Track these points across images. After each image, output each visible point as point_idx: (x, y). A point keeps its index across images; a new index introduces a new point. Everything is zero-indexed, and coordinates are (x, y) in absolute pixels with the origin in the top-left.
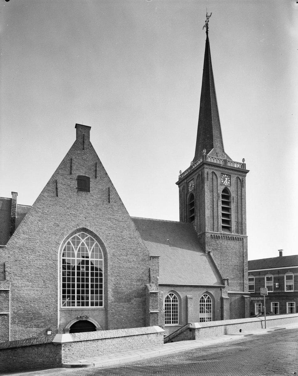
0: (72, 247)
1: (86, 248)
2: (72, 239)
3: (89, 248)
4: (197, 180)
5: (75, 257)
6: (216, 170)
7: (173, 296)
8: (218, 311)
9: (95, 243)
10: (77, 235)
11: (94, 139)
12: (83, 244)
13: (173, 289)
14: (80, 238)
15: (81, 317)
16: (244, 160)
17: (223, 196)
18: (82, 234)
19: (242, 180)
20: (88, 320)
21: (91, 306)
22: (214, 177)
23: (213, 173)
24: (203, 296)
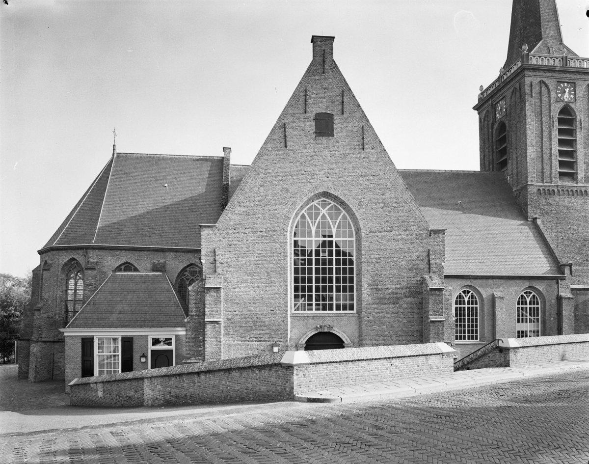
2: (308, 209)
6: (547, 77)
7: (531, 295)
8: (552, 319)
9: (342, 214)
10: (314, 203)
12: (324, 217)
13: (468, 282)
14: (320, 207)
15: (321, 327)
20: (332, 331)
21: (336, 310)
22: (544, 88)
24: (523, 293)
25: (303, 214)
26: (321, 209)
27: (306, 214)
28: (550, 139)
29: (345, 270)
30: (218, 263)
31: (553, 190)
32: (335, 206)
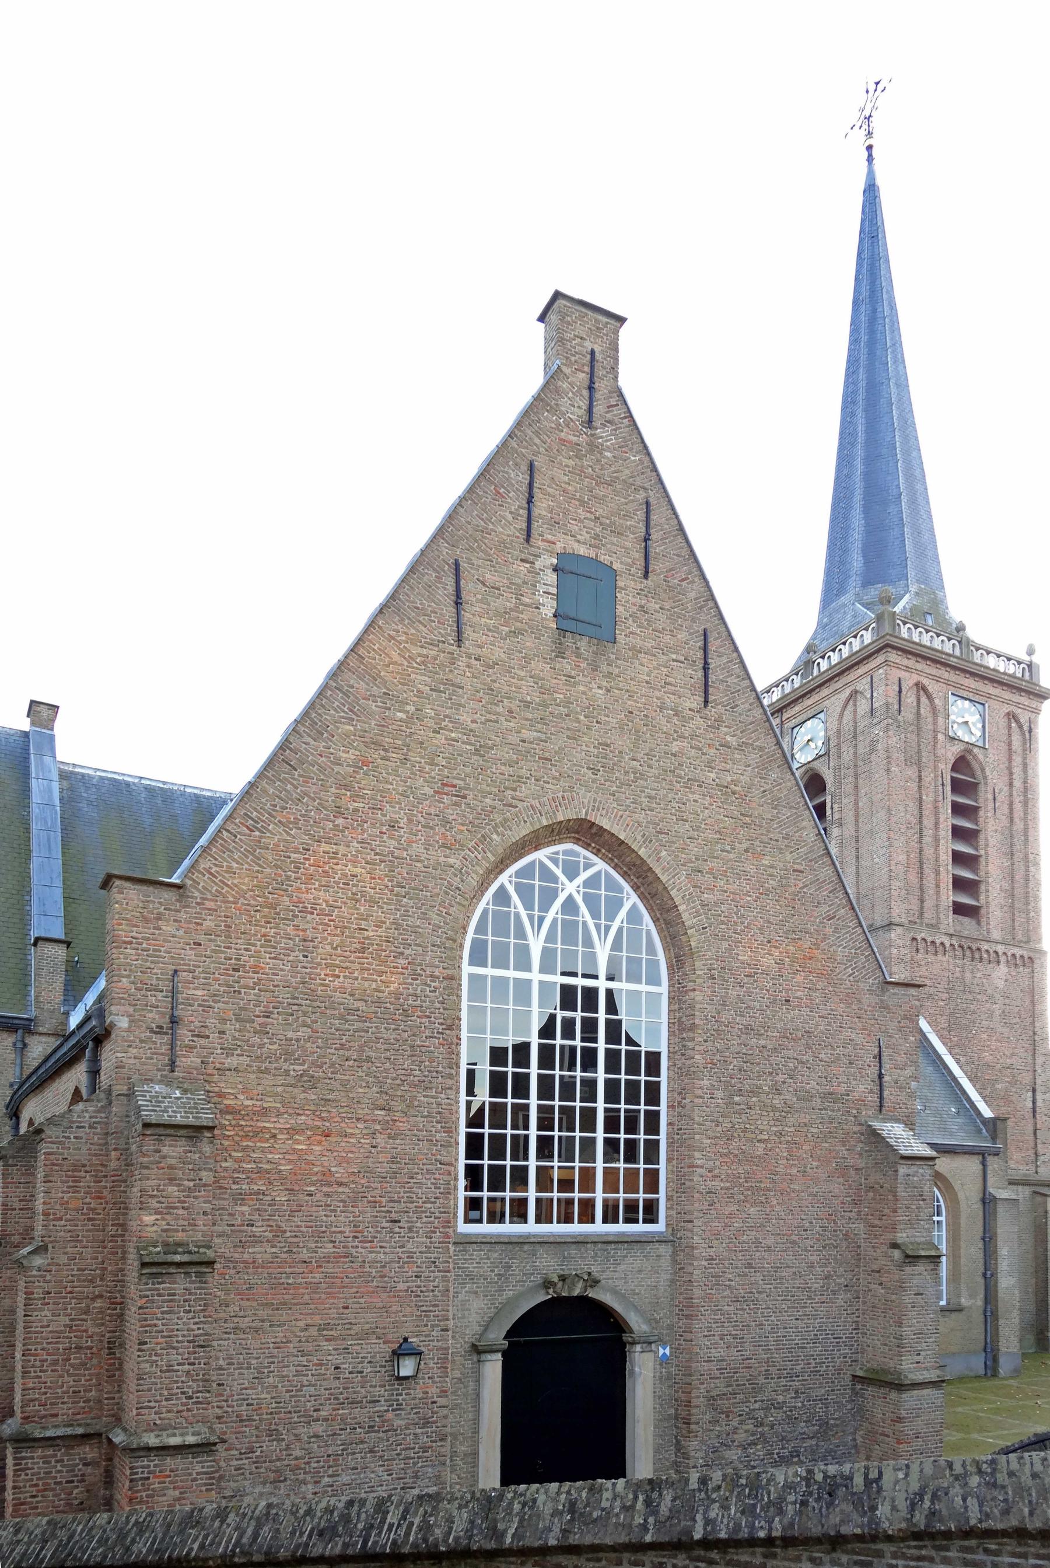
0: (517, 915)
1: (585, 923)
2: (518, 874)
3: (598, 927)
4: (841, 715)
5: (528, 969)
6: (937, 679)
9: (627, 906)
10: (541, 855)
11: (637, 376)
12: (570, 905)
14: (558, 872)
15: (563, 1278)
16: (1031, 652)
17: (957, 786)
18: (565, 853)
19: (1026, 728)
20: (591, 1294)
21: (538, 1221)
22: (924, 699)
23: (920, 687)
25: (502, 888)
26: (562, 878)
27: (511, 889)
28: (937, 824)
29: (633, 1087)
30: (184, 1035)
31: (942, 944)
32: (607, 873)
